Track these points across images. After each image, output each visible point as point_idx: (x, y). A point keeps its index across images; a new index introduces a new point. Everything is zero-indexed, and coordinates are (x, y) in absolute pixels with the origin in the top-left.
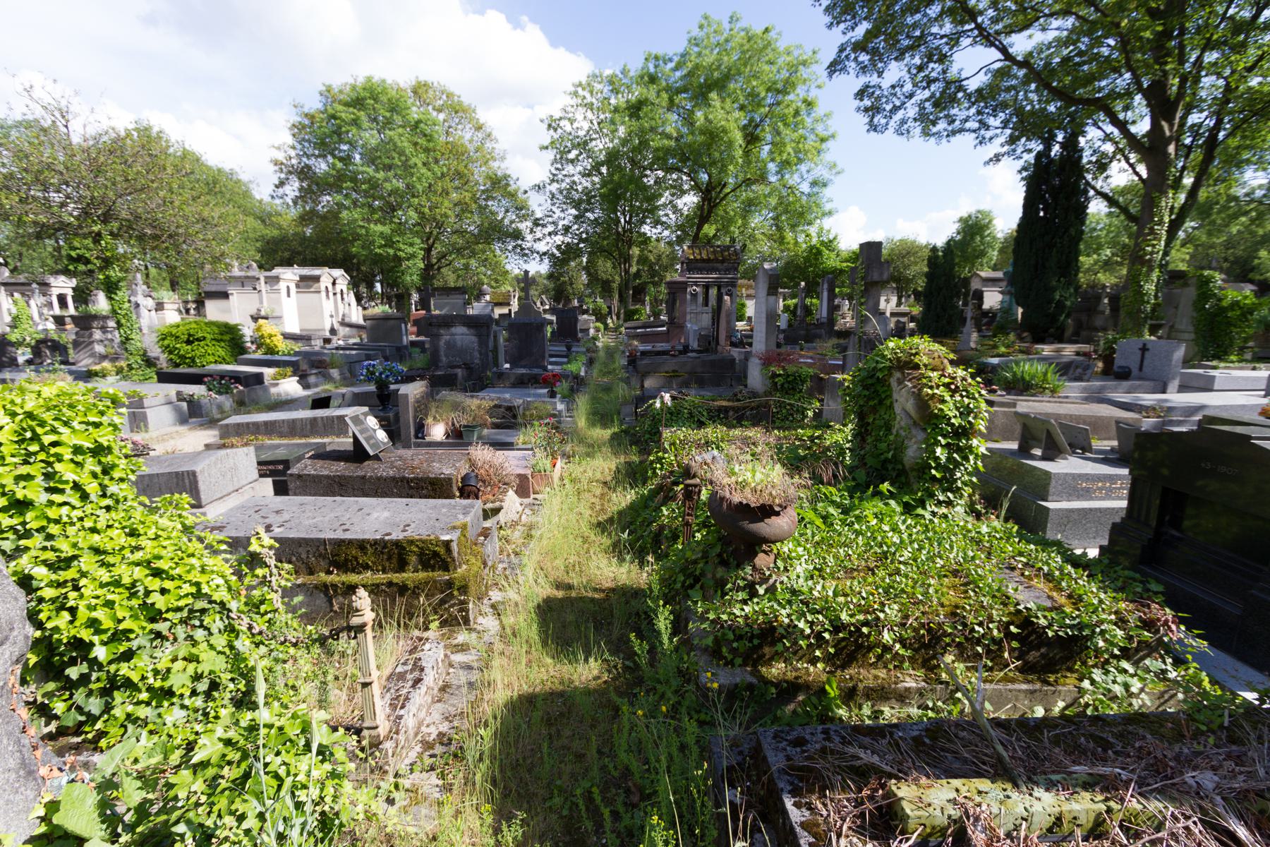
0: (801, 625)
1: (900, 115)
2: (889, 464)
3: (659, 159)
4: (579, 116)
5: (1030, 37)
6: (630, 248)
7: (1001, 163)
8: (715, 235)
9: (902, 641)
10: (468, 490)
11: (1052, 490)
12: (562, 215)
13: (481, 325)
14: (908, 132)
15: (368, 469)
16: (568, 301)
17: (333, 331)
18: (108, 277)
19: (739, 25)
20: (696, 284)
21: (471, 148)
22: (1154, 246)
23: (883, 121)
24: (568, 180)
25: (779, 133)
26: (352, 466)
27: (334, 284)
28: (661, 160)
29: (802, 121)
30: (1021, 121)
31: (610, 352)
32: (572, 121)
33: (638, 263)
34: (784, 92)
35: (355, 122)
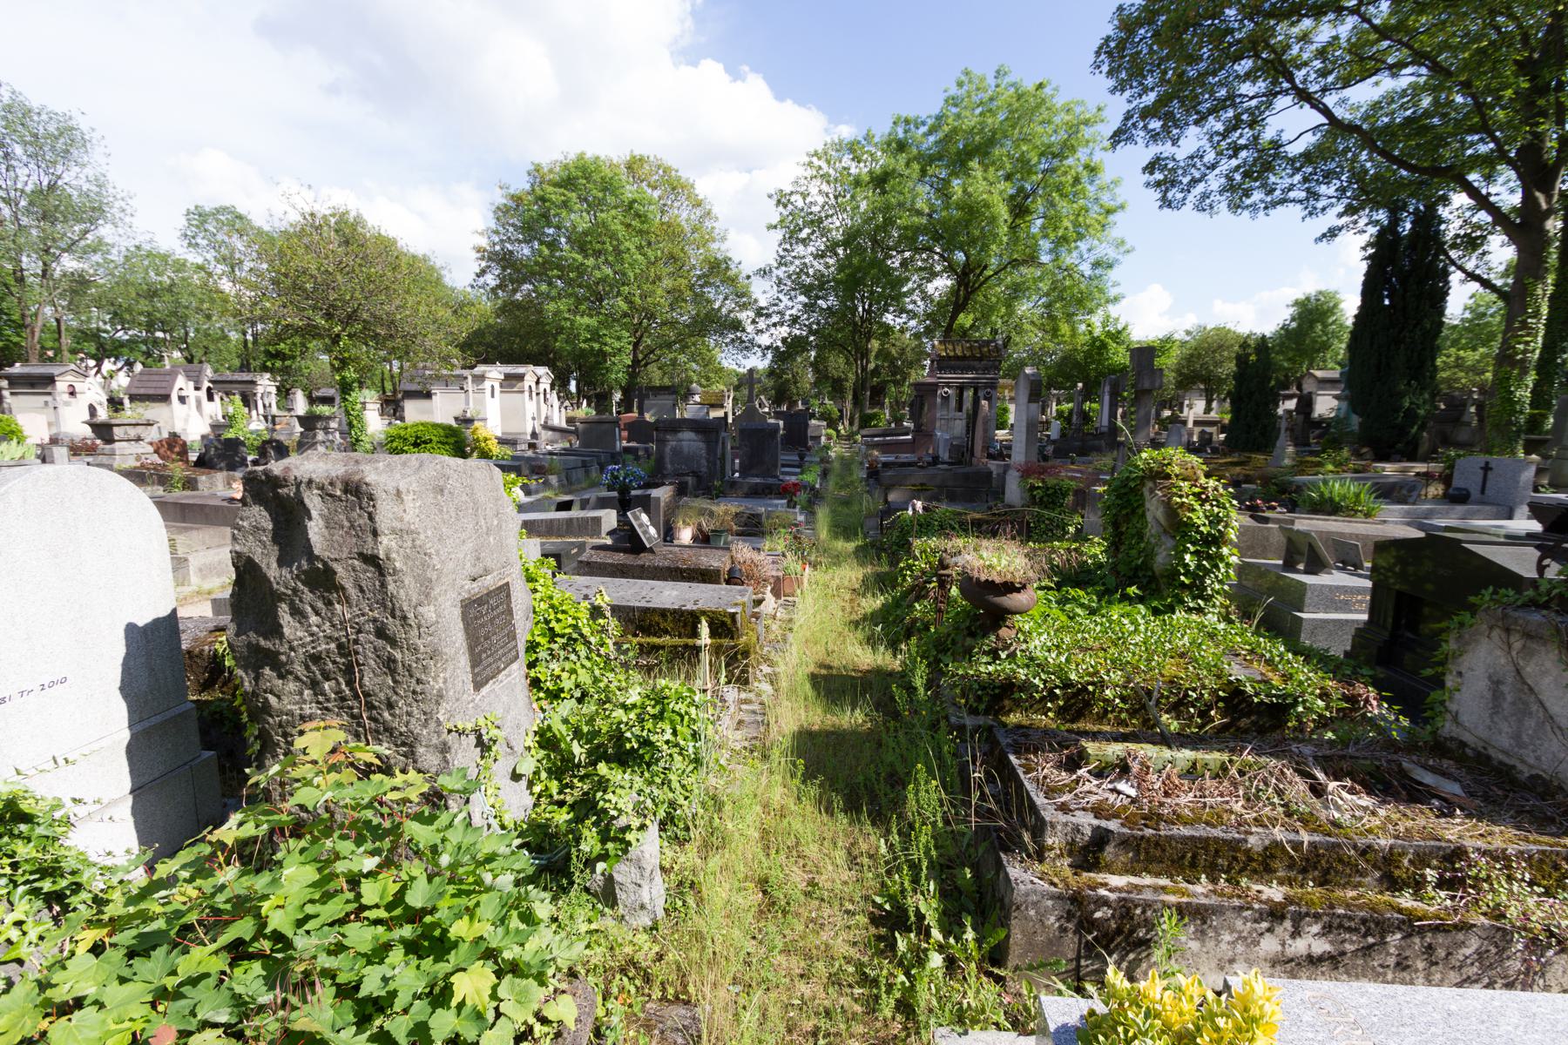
0: (1037, 681)
1: (1200, 188)
2: (1143, 570)
3: (906, 238)
4: (814, 190)
5: (1377, 84)
6: (868, 341)
7: (1337, 239)
8: (972, 326)
9: (1123, 699)
10: (732, 579)
11: (1307, 601)
12: (790, 304)
13: (708, 430)
14: (1211, 207)
15: (644, 559)
16: (793, 404)
17: (534, 435)
18: (343, 378)
19: (1008, 80)
20: (948, 385)
21: (687, 229)
22: (1527, 343)
23: (1180, 196)
24: (797, 262)
25: (1053, 205)
26: (631, 557)
27: (538, 383)
28: (909, 238)
29: (1083, 191)
30: (1362, 190)
31: (846, 464)
32: (804, 196)
33: (877, 357)
34: (1060, 156)
35: (565, 204)
